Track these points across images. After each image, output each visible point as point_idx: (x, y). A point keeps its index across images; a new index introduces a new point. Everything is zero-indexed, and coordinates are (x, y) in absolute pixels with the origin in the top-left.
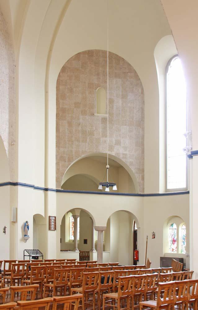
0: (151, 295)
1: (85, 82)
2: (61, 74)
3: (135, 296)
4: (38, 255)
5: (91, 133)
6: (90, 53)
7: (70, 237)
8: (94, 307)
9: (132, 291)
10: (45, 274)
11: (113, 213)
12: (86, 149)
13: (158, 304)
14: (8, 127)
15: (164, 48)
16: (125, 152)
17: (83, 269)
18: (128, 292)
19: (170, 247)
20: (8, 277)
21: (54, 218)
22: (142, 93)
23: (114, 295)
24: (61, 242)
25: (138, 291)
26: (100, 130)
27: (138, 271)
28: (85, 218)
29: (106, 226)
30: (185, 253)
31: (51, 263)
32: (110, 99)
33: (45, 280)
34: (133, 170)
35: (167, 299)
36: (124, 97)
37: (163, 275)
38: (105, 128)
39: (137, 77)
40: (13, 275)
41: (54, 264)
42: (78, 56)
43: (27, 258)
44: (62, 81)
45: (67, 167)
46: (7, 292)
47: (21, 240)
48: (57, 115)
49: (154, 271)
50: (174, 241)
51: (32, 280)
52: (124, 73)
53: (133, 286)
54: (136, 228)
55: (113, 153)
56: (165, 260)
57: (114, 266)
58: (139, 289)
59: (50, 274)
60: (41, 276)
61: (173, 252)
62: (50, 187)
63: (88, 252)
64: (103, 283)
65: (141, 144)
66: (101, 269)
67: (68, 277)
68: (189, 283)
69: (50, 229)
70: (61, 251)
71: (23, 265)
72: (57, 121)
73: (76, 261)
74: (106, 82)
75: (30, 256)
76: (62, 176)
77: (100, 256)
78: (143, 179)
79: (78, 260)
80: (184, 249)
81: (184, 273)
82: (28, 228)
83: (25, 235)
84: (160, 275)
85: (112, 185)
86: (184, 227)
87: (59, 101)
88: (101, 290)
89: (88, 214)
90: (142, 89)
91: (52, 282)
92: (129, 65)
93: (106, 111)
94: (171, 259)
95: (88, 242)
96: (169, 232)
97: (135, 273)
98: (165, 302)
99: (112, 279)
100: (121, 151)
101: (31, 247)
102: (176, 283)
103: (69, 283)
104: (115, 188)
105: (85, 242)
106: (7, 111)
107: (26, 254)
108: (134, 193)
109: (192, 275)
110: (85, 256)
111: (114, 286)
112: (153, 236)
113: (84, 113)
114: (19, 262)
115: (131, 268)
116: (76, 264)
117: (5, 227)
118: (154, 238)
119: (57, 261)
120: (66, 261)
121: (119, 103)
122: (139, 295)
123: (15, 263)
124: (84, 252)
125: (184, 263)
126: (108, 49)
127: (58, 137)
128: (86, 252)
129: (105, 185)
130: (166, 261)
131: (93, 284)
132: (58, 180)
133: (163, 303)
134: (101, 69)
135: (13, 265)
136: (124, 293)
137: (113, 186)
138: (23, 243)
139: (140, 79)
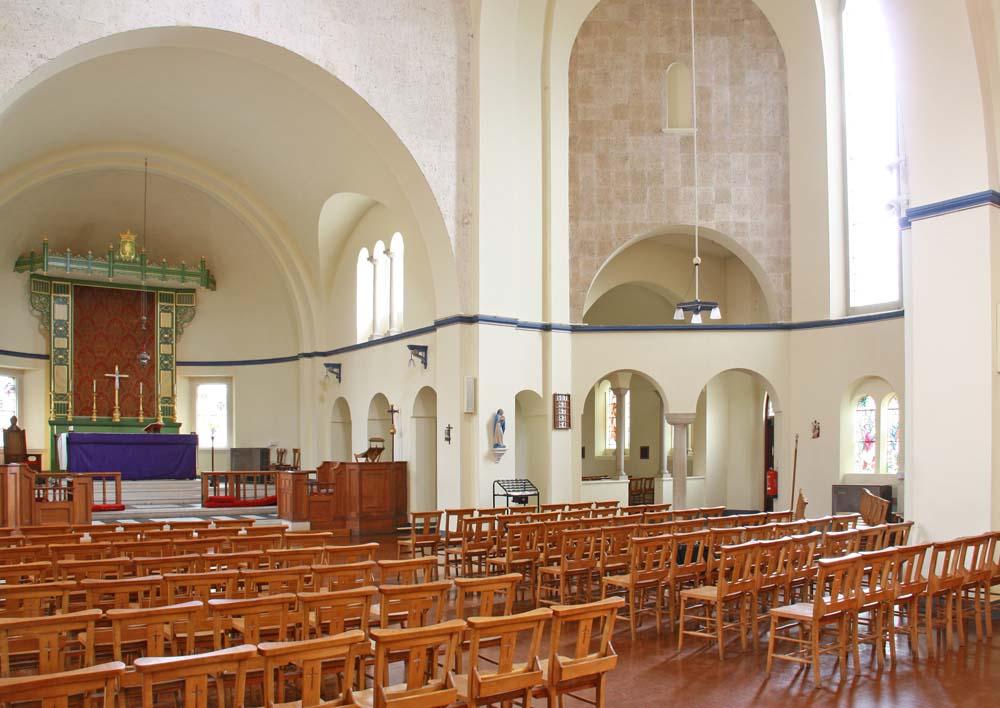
1: (638, 55)
2: (580, 41)
3: (761, 592)
4: (527, 493)
7: (605, 442)
8: (658, 620)
9: (753, 581)
10: (540, 540)
11: (716, 373)
12: (644, 220)
13: (816, 612)
14: (454, 181)
17: (632, 528)
18: (743, 583)
19: (857, 458)
20: (455, 549)
21: (565, 399)
22: (782, 65)
23: (708, 592)
24: (583, 456)
25: (768, 581)
26: (679, 168)
27: (772, 527)
28: (642, 393)
29: (694, 410)
30: (895, 472)
31: (557, 514)
32: (700, 88)
33: (542, 556)
34: (761, 261)
36: (736, 80)
37: (832, 537)
38: (689, 163)
39: (767, 30)
40: (466, 545)
41: (564, 515)
43: (501, 503)
44: (582, 56)
45: (598, 268)
46: (917, 556)
48: (572, 141)
49: (811, 526)
50: (868, 442)
51: (511, 558)
52: (736, 21)
53: (756, 566)
54: (771, 414)
55: (712, 225)
56: (843, 493)
58: (771, 574)
59: (554, 541)
60: (531, 547)
62: (555, 320)
63: (652, 479)
64: (682, 563)
65: (781, 195)
66: (679, 525)
67: (597, 548)
68: (897, 555)
69: (556, 426)
70: (584, 479)
71: (491, 520)
72: (570, 155)
73: (619, 506)
74: (688, 48)
75: (508, 496)
76: (585, 291)
77: (680, 489)
78: (788, 284)
79: (624, 503)
80: (894, 461)
81: (889, 527)
82: (503, 427)
83: (497, 445)
84: (828, 537)
85: (707, 307)
86: (895, 404)
87: (574, 107)
88: (677, 580)
89: (650, 383)
90: (782, 56)
91: (558, 561)
93: (692, 120)
94: (859, 489)
96: (855, 419)
97: (762, 533)
98: (835, 605)
99: (706, 550)
100: (732, 217)
101: (510, 474)
102: (864, 558)
103: (599, 564)
104: (716, 314)
105: (644, 453)
106: (452, 143)
107: (499, 490)
108: (767, 323)
109: (909, 530)
110: (642, 492)
111: (709, 569)
112: (814, 431)
113: (636, 129)
114: (481, 512)
116: (618, 515)
117: (449, 428)
118: (818, 436)
119: (571, 507)
120: (594, 507)
121: (723, 95)
123: (162, 529)
124: (641, 479)
125: (893, 496)
127: (575, 196)
128: (647, 479)
129: (691, 308)
130: (846, 496)
131: (656, 564)
132: (575, 303)
133: (829, 608)
134: (677, 18)
135: (468, 521)
136: (731, 588)
137: (710, 309)
138: (493, 465)
139: (774, 33)
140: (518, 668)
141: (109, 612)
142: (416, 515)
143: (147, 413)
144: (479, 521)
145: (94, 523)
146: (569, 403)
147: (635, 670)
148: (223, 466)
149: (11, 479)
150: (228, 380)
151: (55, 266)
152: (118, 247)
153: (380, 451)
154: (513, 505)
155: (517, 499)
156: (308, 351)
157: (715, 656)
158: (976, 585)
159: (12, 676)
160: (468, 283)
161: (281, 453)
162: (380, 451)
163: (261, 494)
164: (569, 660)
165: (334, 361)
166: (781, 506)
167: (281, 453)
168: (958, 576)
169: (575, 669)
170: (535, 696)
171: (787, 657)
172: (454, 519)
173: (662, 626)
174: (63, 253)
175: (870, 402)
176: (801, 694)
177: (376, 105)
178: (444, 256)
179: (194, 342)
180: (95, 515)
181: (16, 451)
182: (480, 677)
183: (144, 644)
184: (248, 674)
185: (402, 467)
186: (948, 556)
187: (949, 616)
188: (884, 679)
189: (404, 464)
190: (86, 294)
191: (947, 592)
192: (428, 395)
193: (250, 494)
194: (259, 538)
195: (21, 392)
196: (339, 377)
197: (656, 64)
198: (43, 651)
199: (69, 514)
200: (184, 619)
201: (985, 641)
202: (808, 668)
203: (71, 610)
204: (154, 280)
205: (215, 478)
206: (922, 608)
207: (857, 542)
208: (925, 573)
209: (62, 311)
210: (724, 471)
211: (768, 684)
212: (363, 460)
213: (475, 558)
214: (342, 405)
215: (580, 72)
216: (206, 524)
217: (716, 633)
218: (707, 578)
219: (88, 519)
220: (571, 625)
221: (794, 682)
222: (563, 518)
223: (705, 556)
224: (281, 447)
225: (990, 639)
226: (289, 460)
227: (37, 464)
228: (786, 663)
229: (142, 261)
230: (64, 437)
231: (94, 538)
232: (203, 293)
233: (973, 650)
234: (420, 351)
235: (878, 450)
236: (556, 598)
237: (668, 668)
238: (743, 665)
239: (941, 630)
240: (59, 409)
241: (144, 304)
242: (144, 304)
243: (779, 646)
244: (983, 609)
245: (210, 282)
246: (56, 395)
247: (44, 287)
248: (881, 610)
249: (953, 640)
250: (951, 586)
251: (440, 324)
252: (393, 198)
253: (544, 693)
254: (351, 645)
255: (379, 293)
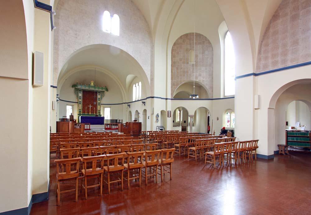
0: (211, 149)
3: (204, 149)
5: (187, 72)
6: (186, 35)
7: (178, 120)
12: (185, 80)
14: (150, 72)
15: (223, 28)
16: (203, 79)
17: (132, 138)
22: (212, 50)
23: (194, 148)
25: (206, 147)
26: (192, 70)
33: (164, 140)
34: (207, 87)
35: (220, 151)
36: (203, 53)
39: (210, 43)
42: (181, 37)
43: (158, 130)
47: (156, 122)
50: (228, 121)
54: (209, 115)
55: (198, 81)
57: (198, 134)
61: (228, 127)
62: (168, 98)
63: (186, 127)
69: (168, 117)
70: (173, 126)
77: (191, 129)
78: (212, 91)
83: (157, 120)
85: (196, 96)
92: (206, 37)
95: (186, 122)
96: (226, 117)
97: (205, 138)
98: (218, 152)
99: (194, 140)
102: (232, 143)
103: (174, 142)
104: (197, 97)
105: (185, 122)
106: (150, 66)
107: (157, 128)
110: (184, 129)
111: (195, 144)
113: (184, 63)
114: (154, 132)
115: (206, 135)
119: (170, 131)
121: (200, 56)
122: (207, 148)
126: (194, 31)
130: (224, 131)
131: (184, 143)
132: (172, 94)
133: (217, 153)
135: (151, 133)
137: (196, 96)
138: (156, 123)
140: (155, 161)
141: (82, 148)
142: (142, 132)
143: (95, 113)
144: (153, 133)
145: (85, 132)
146: (170, 113)
147: (180, 162)
148: (109, 123)
149: (70, 124)
150: (110, 107)
151: (79, 87)
152: (90, 84)
153: (136, 120)
154: (160, 131)
155: (161, 129)
156: (124, 102)
157: (195, 160)
158: (249, 150)
159: (64, 159)
160: (152, 91)
161: (119, 120)
162: (136, 120)
163: (115, 127)
164: (165, 159)
165: (129, 104)
166: (210, 133)
167: (119, 120)
168: (251, 147)
169: (166, 161)
170: (158, 166)
171: (209, 162)
172: (148, 133)
173: (186, 154)
174: (80, 84)
175: (229, 114)
176: (211, 169)
177: (136, 59)
178: (148, 86)
179: (104, 101)
180: (85, 131)
181: (72, 119)
182: (148, 162)
183: (88, 154)
184: (104, 160)
185: (140, 123)
186: (243, 144)
187: (243, 156)
188: (229, 168)
189: (141, 123)
190: (84, 92)
191: (243, 151)
192: (145, 111)
193: (113, 128)
194: (113, 135)
195: (73, 109)
196: (130, 107)
197: (187, 50)
198: (69, 155)
199: (80, 130)
200: (95, 150)
201: (251, 161)
202: (214, 164)
203: (76, 147)
204: (97, 89)
205: (107, 125)
206: (237, 154)
207: (224, 140)
208: (238, 147)
209: (80, 95)
210: (200, 126)
211: (205, 167)
212: (133, 122)
213: (152, 140)
214: (130, 112)
215: (173, 52)
216: (104, 133)
217: (195, 156)
218: (194, 146)
219: (83, 131)
220: (165, 153)
221: (210, 167)
222: (168, 133)
223: (194, 141)
224: (119, 119)
225: (252, 161)
226: (121, 122)
227: (75, 122)
228: (209, 163)
229: (95, 86)
230: (80, 117)
231: (83, 135)
232: (106, 92)
233: (249, 163)
234: (144, 103)
235: (230, 123)
236: (166, 148)
237: (186, 162)
238: (201, 162)
239: (242, 159)
240: (79, 112)
241: (95, 94)
242: (95, 94)
243: (207, 160)
244: (251, 155)
245: (107, 90)
246: (79, 109)
247: (77, 91)
248: (229, 152)
249: (244, 161)
250: (243, 151)
251: (147, 98)
252: (140, 76)
253: (160, 165)
254: (124, 155)
255: (137, 92)
